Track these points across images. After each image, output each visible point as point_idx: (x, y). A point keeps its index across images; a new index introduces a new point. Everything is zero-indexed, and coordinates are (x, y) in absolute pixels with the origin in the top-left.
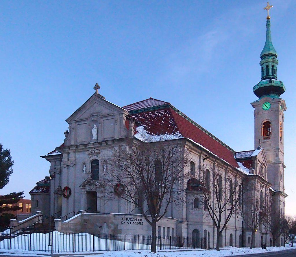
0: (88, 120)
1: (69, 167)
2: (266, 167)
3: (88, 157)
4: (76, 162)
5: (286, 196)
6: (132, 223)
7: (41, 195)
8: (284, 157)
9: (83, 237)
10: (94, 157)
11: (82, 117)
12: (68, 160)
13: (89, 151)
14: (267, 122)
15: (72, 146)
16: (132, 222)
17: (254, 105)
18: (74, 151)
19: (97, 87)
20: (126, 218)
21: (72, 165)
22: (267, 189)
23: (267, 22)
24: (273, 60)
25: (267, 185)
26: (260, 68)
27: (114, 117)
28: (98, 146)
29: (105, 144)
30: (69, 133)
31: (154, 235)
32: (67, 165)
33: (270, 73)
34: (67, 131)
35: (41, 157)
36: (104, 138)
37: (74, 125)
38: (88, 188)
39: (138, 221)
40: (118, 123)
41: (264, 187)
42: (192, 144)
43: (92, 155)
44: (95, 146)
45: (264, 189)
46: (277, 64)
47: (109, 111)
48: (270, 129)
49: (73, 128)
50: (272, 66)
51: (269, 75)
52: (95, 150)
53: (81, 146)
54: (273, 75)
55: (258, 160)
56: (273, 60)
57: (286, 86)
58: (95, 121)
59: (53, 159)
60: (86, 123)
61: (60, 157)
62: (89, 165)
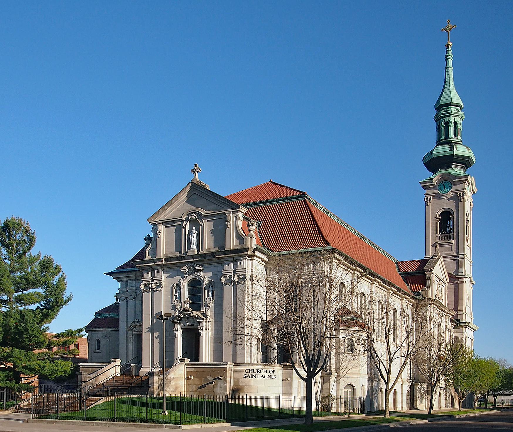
2: (447, 285)
6: (260, 376)
22: (447, 320)
24: (456, 113)
26: (435, 125)
30: (153, 239)
31: (310, 397)
34: (149, 235)
35: (104, 273)
39: (268, 374)
41: (444, 316)
48: (450, 223)
55: (434, 275)
59: (125, 277)
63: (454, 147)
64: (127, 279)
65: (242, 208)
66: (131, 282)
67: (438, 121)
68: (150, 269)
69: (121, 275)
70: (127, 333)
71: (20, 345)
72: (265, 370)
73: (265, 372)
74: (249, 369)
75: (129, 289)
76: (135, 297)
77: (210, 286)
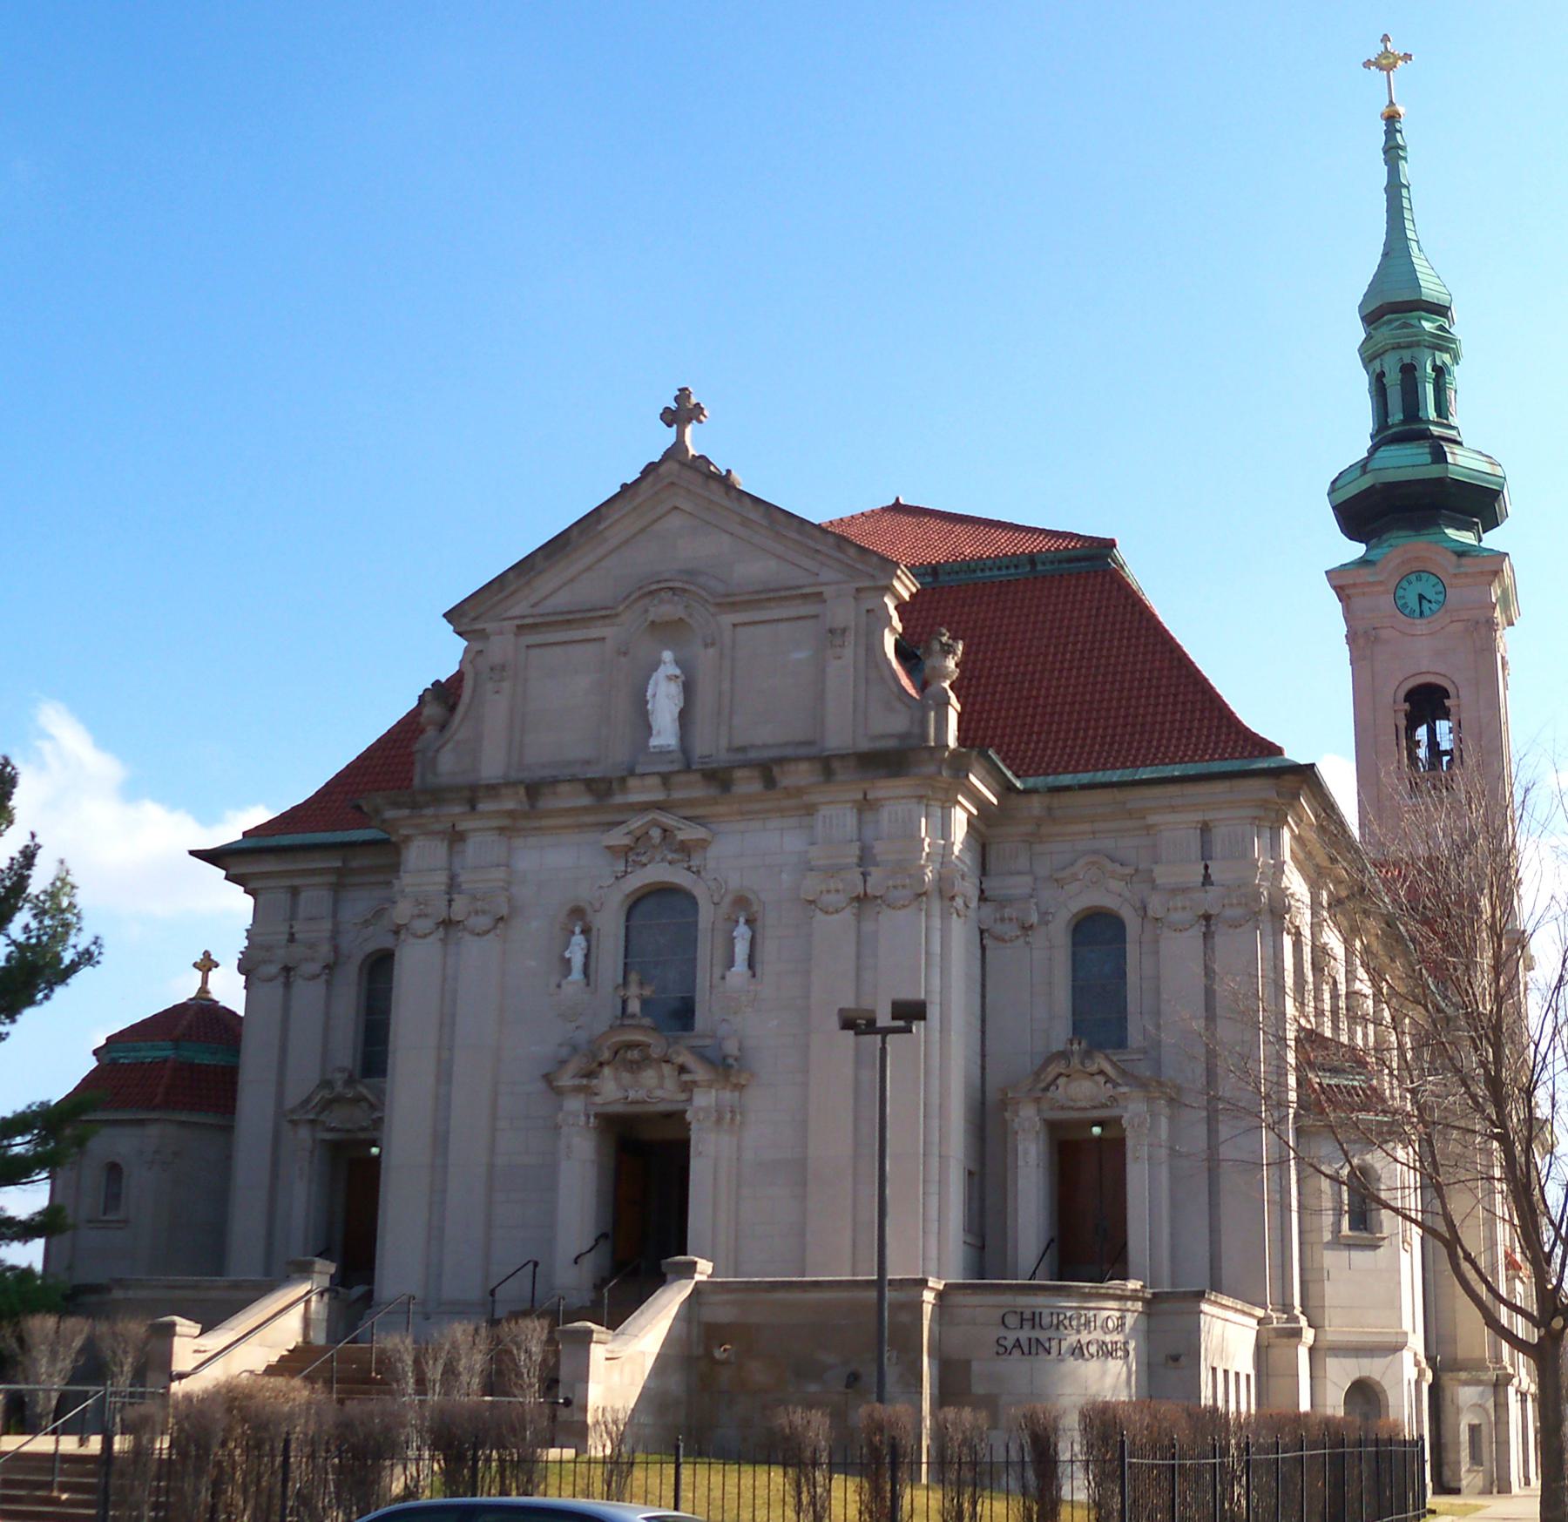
0: (617, 615)
4: (510, 900)
7: (153, 1131)
10: (657, 872)
11: (562, 600)
13: (623, 829)
15: (493, 790)
18: (506, 822)
19: (682, 412)
20: (1027, 1315)
21: (483, 922)
23: (1386, 132)
29: (757, 787)
32: (443, 922)
35: (192, 853)
36: (737, 743)
37: (502, 646)
40: (849, 652)
43: (644, 859)
44: (677, 795)
46: (1456, 359)
47: (773, 564)
49: (503, 667)
50: (1435, 368)
51: (1420, 420)
52: (668, 820)
53: (564, 788)
58: (668, 631)
60: (603, 639)
61: (339, 864)
62: (610, 924)
64: (297, 882)
65: (903, 577)
66: (315, 899)
67: (1375, 358)
68: (444, 832)
69: (270, 865)
71: (1481, 1100)
74: (1019, 1310)
76: (330, 967)
77: (742, 920)
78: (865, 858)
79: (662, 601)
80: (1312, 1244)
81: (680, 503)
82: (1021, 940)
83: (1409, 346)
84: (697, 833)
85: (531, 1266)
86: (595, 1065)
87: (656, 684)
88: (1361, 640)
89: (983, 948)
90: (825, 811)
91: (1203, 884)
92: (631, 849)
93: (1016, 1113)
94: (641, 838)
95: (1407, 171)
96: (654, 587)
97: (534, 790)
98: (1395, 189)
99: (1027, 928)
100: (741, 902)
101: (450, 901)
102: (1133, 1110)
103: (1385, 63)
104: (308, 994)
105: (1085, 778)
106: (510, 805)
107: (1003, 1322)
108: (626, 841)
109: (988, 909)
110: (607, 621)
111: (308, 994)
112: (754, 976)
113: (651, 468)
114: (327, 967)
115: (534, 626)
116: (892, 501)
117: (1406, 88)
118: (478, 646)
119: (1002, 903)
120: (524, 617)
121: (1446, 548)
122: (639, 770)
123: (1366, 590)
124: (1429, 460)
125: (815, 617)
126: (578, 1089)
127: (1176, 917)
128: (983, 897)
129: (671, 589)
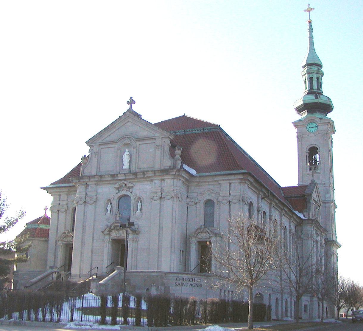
0: (118, 142)
1: (87, 204)
2: (320, 208)
3: (115, 191)
4: (97, 198)
5: (339, 246)
6: (189, 285)
8: (335, 194)
9: (93, 302)
10: (124, 192)
11: (108, 139)
12: (86, 194)
14: (314, 147)
15: (93, 177)
16: (190, 283)
17: (296, 124)
19: (131, 102)
20: (181, 278)
24: (318, 71)
25: (322, 232)
27: (155, 141)
28: (131, 177)
33: (315, 87)
36: (139, 168)
38: (114, 234)
39: (196, 282)
42: (254, 179)
43: (121, 190)
44: (127, 178)
45: (319, 237)
46: (322, 75)
51: (314, 89)
52: (126, 182)
54: (318, 89)
55: (313, 198)
56: (318, 71)
57: (335, 103)
58: (128, 145)
61: (68, 190)
62: (115, 202)
63: (318, 97)
64: (230, 182)
66: (64, 197)
69: (55, 190)
70: (56, 242)
72: (194, 279)
73: (193, 281)
75: (61, 203)
77: (139, 202)
78: (162, 190)
79: (126, 140)
80: (102, 272)
81: (130, 120)
82: (194, 206)
83: (312, 73)
84: (131, 185)
85: (97, 268)
86: (111, 230)
87: (124, 156)
88: (300, 137)
89: (187, 207)
90: (154, 181)
91: (229, 195)
92: (119, 188)
93: (191, 239)
94: (121, 186)
95: (314, 34)
96: (124, 137)
97: (101, 177)
98: (311, 38)
99: (196, 203)
100: (139, 198)
101: (86, 198)
102: (213, 239)
103: (310, 10)
104: (62, 215)
105: (207, 174)
106: (97, 179)
107: (176, 279)
108: (118, 186)
109: (188, 200)
110: (116, 144)
111: (62, 215)
112: (141, 213)
113: (124, 113)
114: (66, 210)
115: (102, 144)
116: (183, 115)
117: (314, 15)
118: (92, 148)
119: (191, 198)
120: (100, 143)
121: (317, 117)
122: (121, 173)
123: (301, 126)
124: (314, 98)
125: (154, 143)
126: (108, 234)
127: (223, 202)
128: (187, 197)
129: (128, 137)
